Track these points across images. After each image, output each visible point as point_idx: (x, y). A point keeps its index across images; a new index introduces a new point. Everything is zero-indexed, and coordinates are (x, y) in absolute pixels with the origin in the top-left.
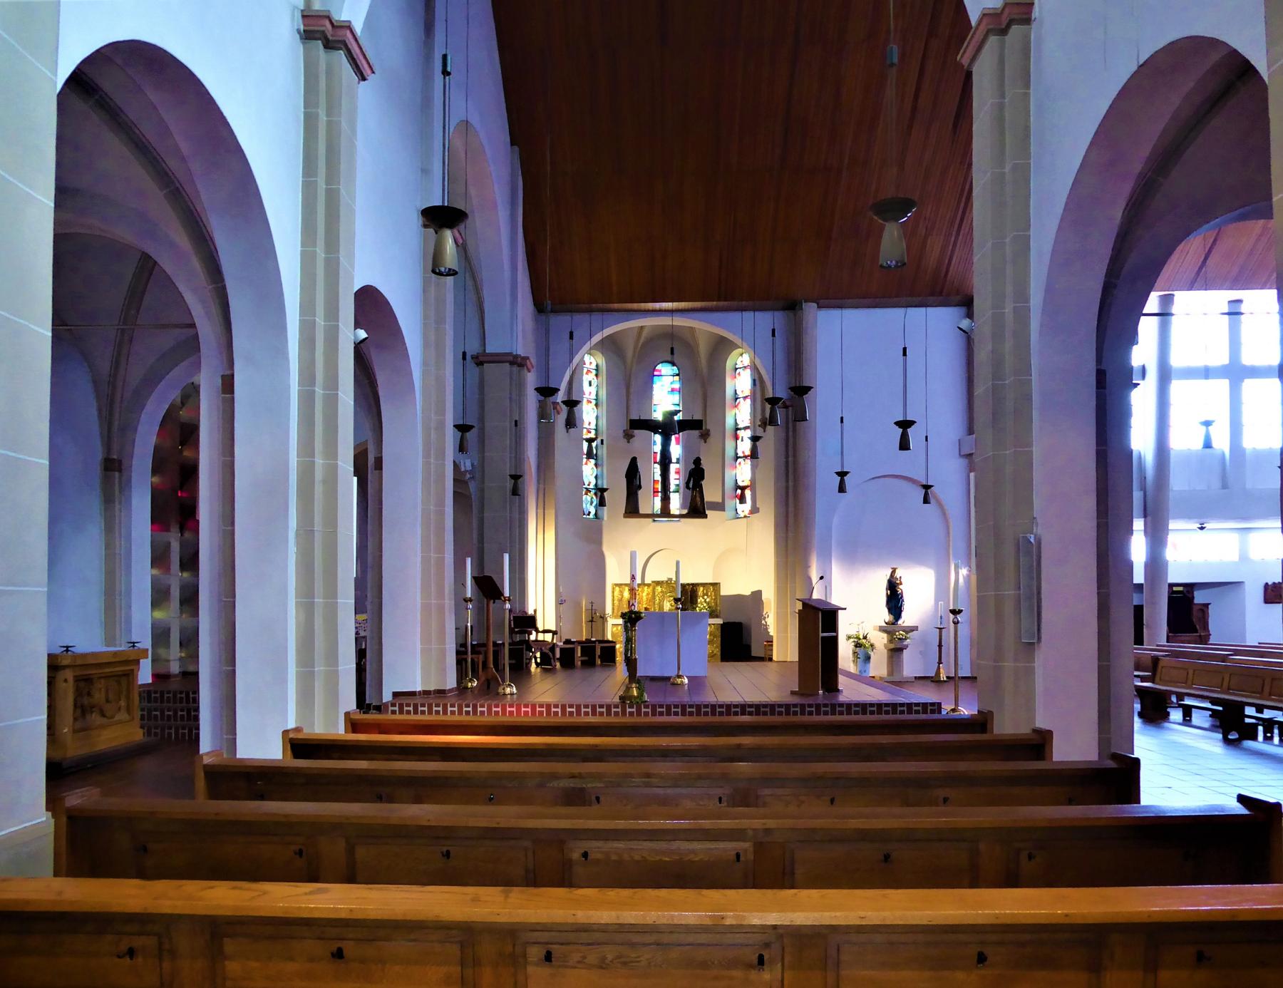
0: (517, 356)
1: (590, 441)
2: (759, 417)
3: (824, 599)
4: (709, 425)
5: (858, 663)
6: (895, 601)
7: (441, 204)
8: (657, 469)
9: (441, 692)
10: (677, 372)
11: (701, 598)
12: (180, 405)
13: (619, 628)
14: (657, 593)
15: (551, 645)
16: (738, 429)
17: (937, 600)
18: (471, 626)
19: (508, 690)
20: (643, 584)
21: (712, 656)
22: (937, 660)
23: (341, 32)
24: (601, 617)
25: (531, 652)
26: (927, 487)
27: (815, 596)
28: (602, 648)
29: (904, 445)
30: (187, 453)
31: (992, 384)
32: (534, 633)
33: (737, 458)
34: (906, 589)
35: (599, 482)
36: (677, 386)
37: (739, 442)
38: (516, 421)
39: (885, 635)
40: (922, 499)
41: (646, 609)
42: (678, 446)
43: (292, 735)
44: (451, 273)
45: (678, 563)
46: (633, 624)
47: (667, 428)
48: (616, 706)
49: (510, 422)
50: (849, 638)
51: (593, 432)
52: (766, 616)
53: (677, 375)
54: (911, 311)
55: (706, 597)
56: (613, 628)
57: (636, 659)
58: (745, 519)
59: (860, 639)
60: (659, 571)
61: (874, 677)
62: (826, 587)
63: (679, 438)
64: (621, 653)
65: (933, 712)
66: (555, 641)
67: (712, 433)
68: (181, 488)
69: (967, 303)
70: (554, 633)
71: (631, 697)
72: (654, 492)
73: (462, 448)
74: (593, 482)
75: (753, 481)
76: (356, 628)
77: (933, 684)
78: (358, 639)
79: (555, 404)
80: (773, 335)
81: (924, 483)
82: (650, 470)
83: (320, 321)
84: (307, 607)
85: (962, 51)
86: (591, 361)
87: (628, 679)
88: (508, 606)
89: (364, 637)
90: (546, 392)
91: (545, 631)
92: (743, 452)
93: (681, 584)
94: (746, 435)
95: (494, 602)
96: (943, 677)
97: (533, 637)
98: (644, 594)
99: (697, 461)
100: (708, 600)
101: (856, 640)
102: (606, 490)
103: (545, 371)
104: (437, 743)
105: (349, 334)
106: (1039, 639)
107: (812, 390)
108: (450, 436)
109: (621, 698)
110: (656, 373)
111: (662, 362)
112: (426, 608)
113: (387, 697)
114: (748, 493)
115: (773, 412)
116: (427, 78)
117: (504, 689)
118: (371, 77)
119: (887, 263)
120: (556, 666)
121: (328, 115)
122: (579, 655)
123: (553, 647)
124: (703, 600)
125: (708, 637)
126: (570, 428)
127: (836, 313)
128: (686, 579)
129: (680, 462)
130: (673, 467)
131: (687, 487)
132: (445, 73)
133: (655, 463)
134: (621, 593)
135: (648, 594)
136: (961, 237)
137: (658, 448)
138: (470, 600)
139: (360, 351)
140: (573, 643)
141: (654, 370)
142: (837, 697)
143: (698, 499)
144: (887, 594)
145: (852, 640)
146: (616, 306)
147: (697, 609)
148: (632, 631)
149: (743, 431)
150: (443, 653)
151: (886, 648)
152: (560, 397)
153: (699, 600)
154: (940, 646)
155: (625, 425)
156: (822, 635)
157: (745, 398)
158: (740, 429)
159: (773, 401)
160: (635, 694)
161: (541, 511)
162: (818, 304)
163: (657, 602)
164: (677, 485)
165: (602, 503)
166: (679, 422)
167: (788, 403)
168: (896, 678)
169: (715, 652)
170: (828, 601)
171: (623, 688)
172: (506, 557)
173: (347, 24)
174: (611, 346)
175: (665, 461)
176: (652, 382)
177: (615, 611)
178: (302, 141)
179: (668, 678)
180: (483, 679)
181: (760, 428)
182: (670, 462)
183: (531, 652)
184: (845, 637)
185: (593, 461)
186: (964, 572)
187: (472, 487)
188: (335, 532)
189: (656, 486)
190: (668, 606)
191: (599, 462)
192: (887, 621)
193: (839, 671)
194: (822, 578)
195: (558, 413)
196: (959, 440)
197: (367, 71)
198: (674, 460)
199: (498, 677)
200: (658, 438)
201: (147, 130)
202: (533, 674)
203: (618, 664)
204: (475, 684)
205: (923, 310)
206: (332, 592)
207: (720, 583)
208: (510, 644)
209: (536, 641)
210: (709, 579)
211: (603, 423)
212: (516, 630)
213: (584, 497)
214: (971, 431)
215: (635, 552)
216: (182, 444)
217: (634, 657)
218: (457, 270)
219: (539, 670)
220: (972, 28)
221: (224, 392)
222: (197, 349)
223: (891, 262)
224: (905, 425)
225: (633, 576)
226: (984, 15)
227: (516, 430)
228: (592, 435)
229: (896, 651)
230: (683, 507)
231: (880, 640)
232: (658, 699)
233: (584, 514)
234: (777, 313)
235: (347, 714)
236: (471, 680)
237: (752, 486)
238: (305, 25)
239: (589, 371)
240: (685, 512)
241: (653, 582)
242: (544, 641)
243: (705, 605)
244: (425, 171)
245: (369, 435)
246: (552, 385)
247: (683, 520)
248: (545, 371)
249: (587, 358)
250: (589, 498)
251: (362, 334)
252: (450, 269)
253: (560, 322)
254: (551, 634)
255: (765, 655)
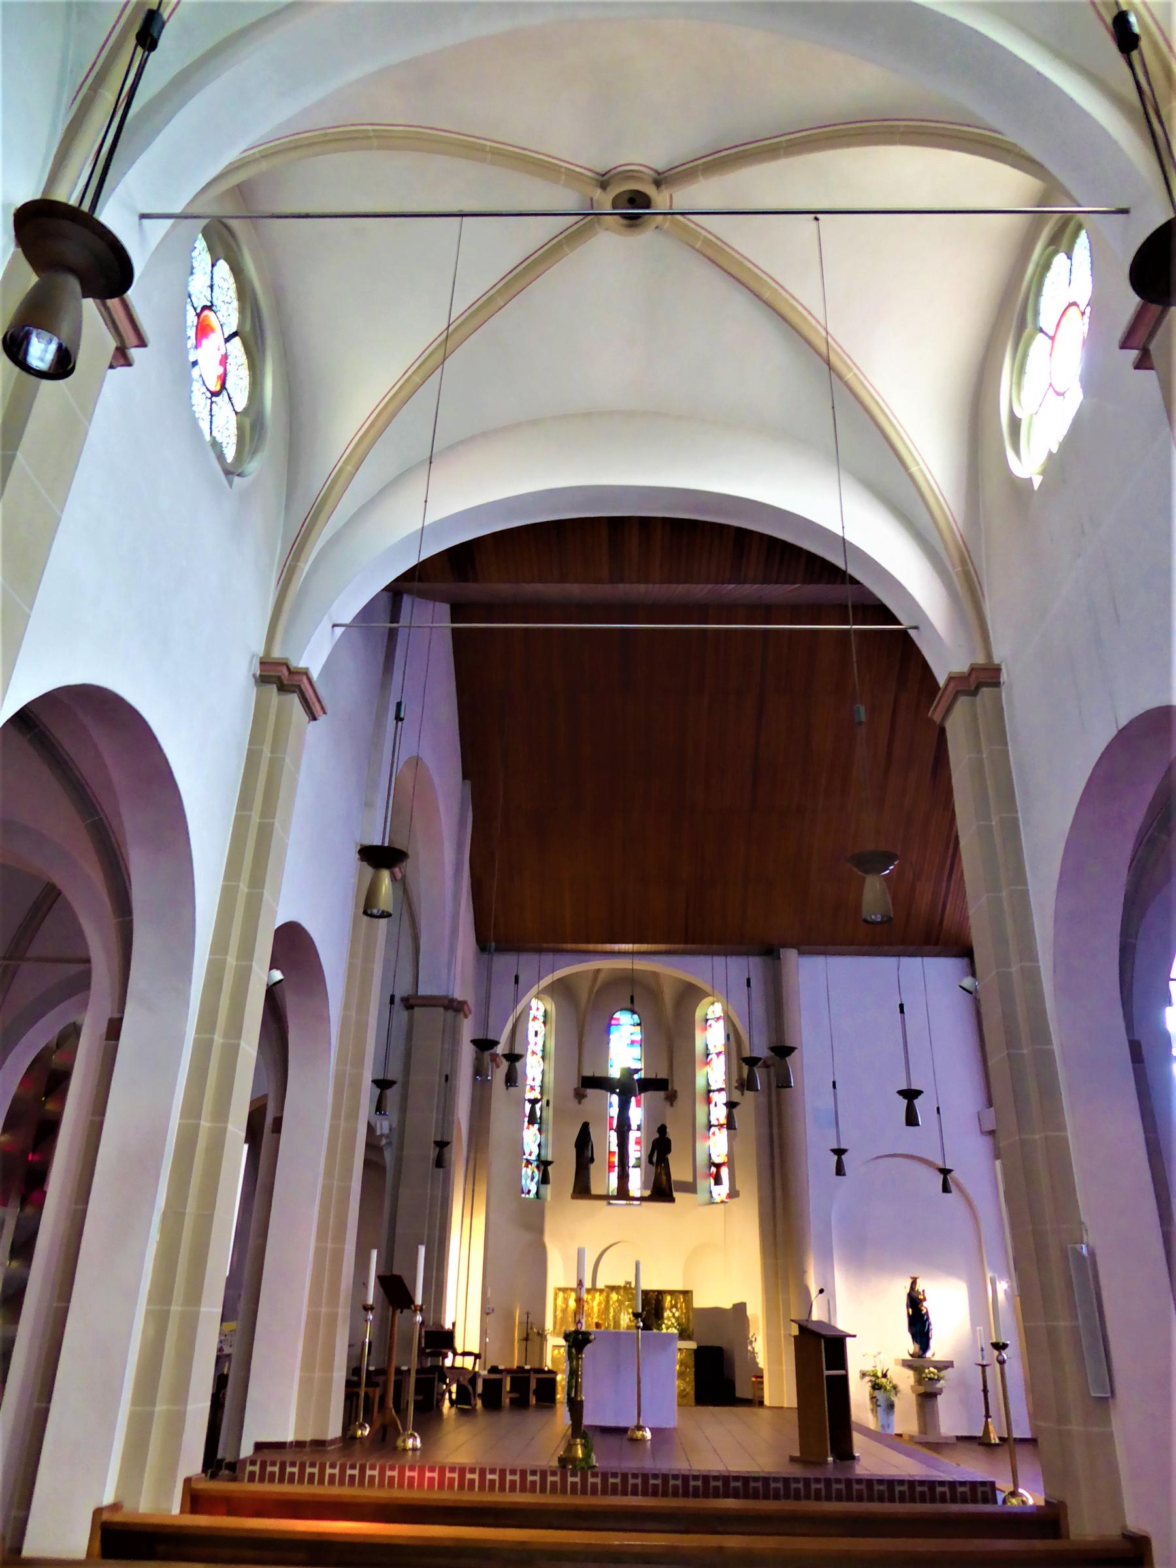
0: (452, 1001)
1: (534, 1102)
2: (735, 1077)
3: (825, 1320)
4: (677, 1085)
5: (879, 1414)
6: (919, 1326)
7: (380, 844)
8: (613, 1137)
9: (319, 1445)
10: (639, 1022)
11: (668, 1311)
12: (55, 1047)
13: (562, 1350)
14: (611, 1302)
15: (472, 1374)
16: (709, 1091)
17: (974, 1324)
18: (370, 1343)
19: (410, 1443)
20: (593, 1289)
21: (682, 1395)
22: (984, 1413)
23: (297, 677)
24: (539, 1334)
25: (445, 1383)
26: (945, 1172)
27: (815, 1316)
28: (538, 1380)
29: (911, 1119)
30: (50, 1106)
31: (1008, 1054)
32: (450, 1355)
33: (710, 1126)
34: (930, 1306)
35: (543, 1152)
36: (638, 1037)
37: (712, 1106)
38: (447, 1076)
39: (910, 1373)
40: (941, 1187)
41: (598, 1325)
42: (639, 1109)
43: (106, 1517)
44: (385, 915)
45: (637, 1265)
46: (580, 1350)
47: (627, 1088)
48: (554, 1473)
49: (440, 1077)
50: (864, 1375)
51: (538, 1089)
52: (753, 1339)
53: (638, 1025)
54: (905, 961)
55: (674, 1310)
56: (554, 1350)
57: (582, 1402)
58: (722, 1205)
59: (878, 1377)
60: (614, 1273)
61: (900, 1435)
62: (829, 1301)
63: (640, 1100)
64: (563, 1388)
65: (985, 1500)
66: (477, 1369)
67: (679, 1095)
68: (34, 1151)
69: (965, 951)
70: (477, 1356)
71: (574, 1460)
72: (609, 1167)
73: (380, 1107)
74: (536, 1151)
75: (730, 1155)
76: (221, 1342)
77: (982, 1448)
78: (221, 1359)
79: (494, 1057)
80: (749, 985)
81: (942, 1166)
82: (605, 1139)
83: (231, 960)
84: (159, 1319)
85: (932, 708)
86: (538, 1007)
87: (570, 1430)
88: (419, 1318)
89: (229, 1356)
90: (484, 1045)
91: (465, 1354)
92: (718, 1120)
93: (643, 1291)
94: (720, 1098)
95: (401, 1312)
96: (995, 1440)
97: (448, 1362)
98: (595, 1303)
99: (662, 1130)
100: (677, 1314)
101: (873, 1379)
102: (550, 1163)
103: (484, 1022)
104: (304, 1533)
105: (263, 975)
106: (1112, 1391)
107: (796, 1051)
108: (367, 1094)
109: (561, 1460)
110: (613, 1022)
111: (621, 1010)
112: (313, 1319)
113: (247, 1450)
114: (724, 1172)
115: (751, 1074)
116: (379, 724)
117: (404, 1441)
118: (322, 718)
119: (871, 918)
120: (475, 1405)
121: (272, 752)
122: (508, 1388)
123: (475, 1375)
124: (671, 1315)
125: (678, 1367)
126: (511, 1086)
127: (820, 961)
128: (650, 1283)
129: (642, 1129)
130: (633, 1135)
131: (650, 1161)
132: (398, 718)
133: (611, 1129)
134: (566, 1300)
135: (600, 1304)
136: (953, 883)
137: (614, 1111)
138: (372, 1308)
139: (273, 994)
140: (501, 1372)
141: (612, 1018)
142: (852, 1468)
143: (664, 1178)
144: (908, 1313)
145: (867, 1379)
146: (569, 946)
147: (664, 1326)
148: (578, 1359)
149: (717, 1093)
150: (327, 1383)
151: (913, 1392)
152: (500, 1049)
153: (665, 1315)
154: (985, 1391)
155: (574, 1083)
156: (827, 1373)
157: (718, 1054)
158: (714, 1091)
159: (751, 1062)
160: (580, 1453)
161: (470, 1187)
162: (798, 950)
163: (611, 1314)
164: (638, 1159)
165: (545, 1180)
166: (639, 1080)
167: (769, 1062)
168: (931, 1438)
169: (688, 1390)
170: (832, 1324)
171: (564, 1445)
172: (422, 1250)
173: (305, 671)
174: (562, 991)
175: (623, 1129)
176: (608, 1032)
177: (558, 1327)
178: (242, 776)
179: (624, 1430)
180: (377, 1425)
181: (737, 1091)
182: (629, 1128)
183: (445, 1383)
184: (858, 1375)
185: (536, 1126)
186: (1002, 1286)
187: (388, 1157)
188: (210, 1217)
189: (612, 1160)
190: (625, 1319)
191: (544, 1127)
192: (911, 1352)
193: (853, 1426)
194: (821, 1291)
195: (498, 1066)
196: (978, 1113)
197: (317, 708)
198: (634, 1126)
199: (399, 1422)
200: (615, 1099)
201: (84, 765)
202: (445, 1417)
203: (558, 1406)
204: (366, 1433)
205: (919, 959)
206: (194, 1295)
207: (692, 1292)
208: (418, 1372)
209: (453, 1367)
210: (679, 1286)
211: (550, 1078)
212: (428, 1351)
213: (524, 1169)
214: (990, 1103)
215: (584, 1249)
216: (48, 1094)
217: (579, 1399)
218: (392, 912)
219: (453, 1410)
220: (939, 689)
221: (107, 1039)
222: (87, 986)
223: (876, 916)
224: (910, 1095)
225: (580, 1281)
226: (951, 679)
227: (446, 1085)
228: (536, 1094)
229: (927, 1397)
230: (644, 1186)
231: (904, 1379)
232: (613, 1465)
233: (523, 1193)
234: (751, 959)
235: (188, 1481)
236: (362, 1427)
237: (730, 1163)
238: (261, 671)
239: (535, 1018)
240: (647, 1193)
241: (607, 1287)
242: (463, 1368)
243: (673, 1321)
244: (368, 805)
245: (270, 1090)
246: (491, 1037)
247: (645, 1204)
248: (484, 1022)
249: (534, 1003)
250: (530, 1173)
251: (277, 975)
252: (383, 912)
253: (504, 963)
254: (472, 1358)
255: (754, 1396)
